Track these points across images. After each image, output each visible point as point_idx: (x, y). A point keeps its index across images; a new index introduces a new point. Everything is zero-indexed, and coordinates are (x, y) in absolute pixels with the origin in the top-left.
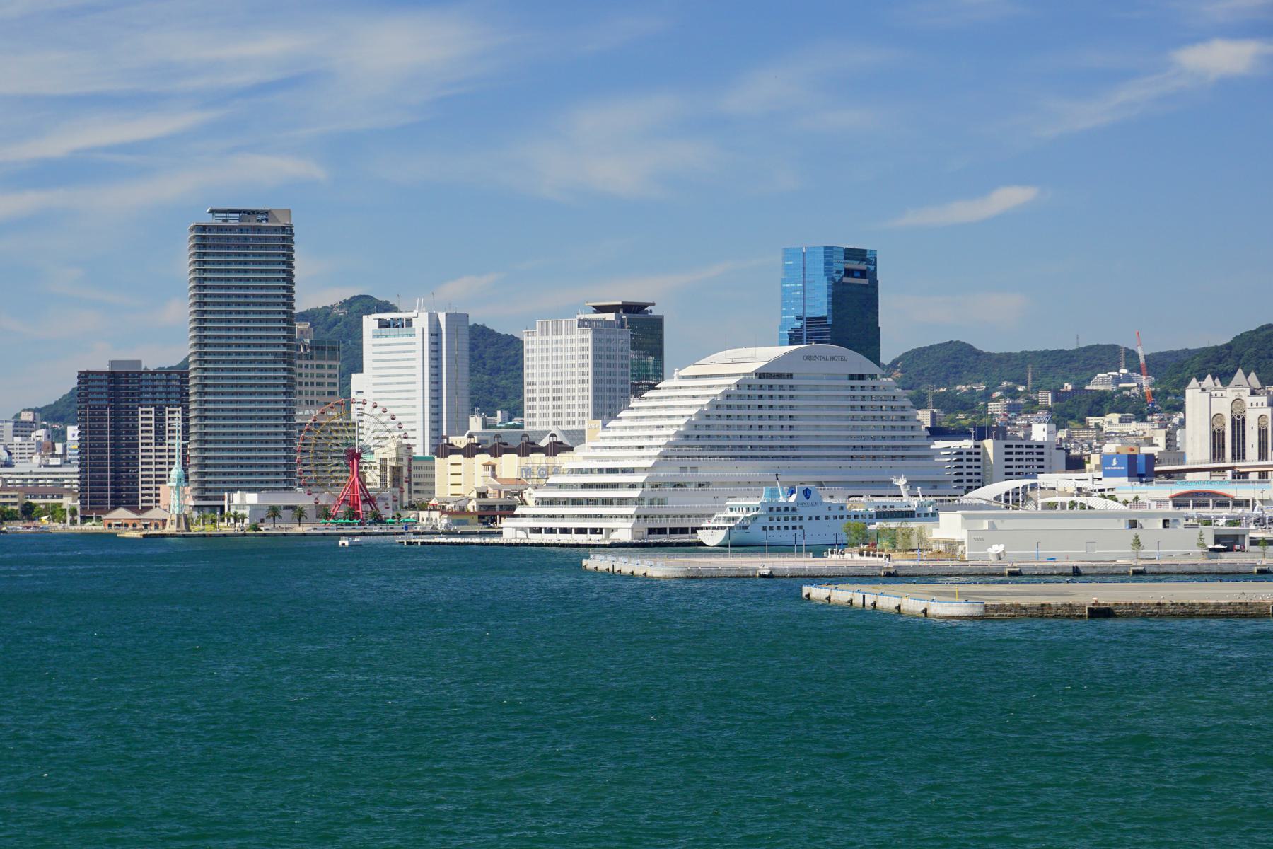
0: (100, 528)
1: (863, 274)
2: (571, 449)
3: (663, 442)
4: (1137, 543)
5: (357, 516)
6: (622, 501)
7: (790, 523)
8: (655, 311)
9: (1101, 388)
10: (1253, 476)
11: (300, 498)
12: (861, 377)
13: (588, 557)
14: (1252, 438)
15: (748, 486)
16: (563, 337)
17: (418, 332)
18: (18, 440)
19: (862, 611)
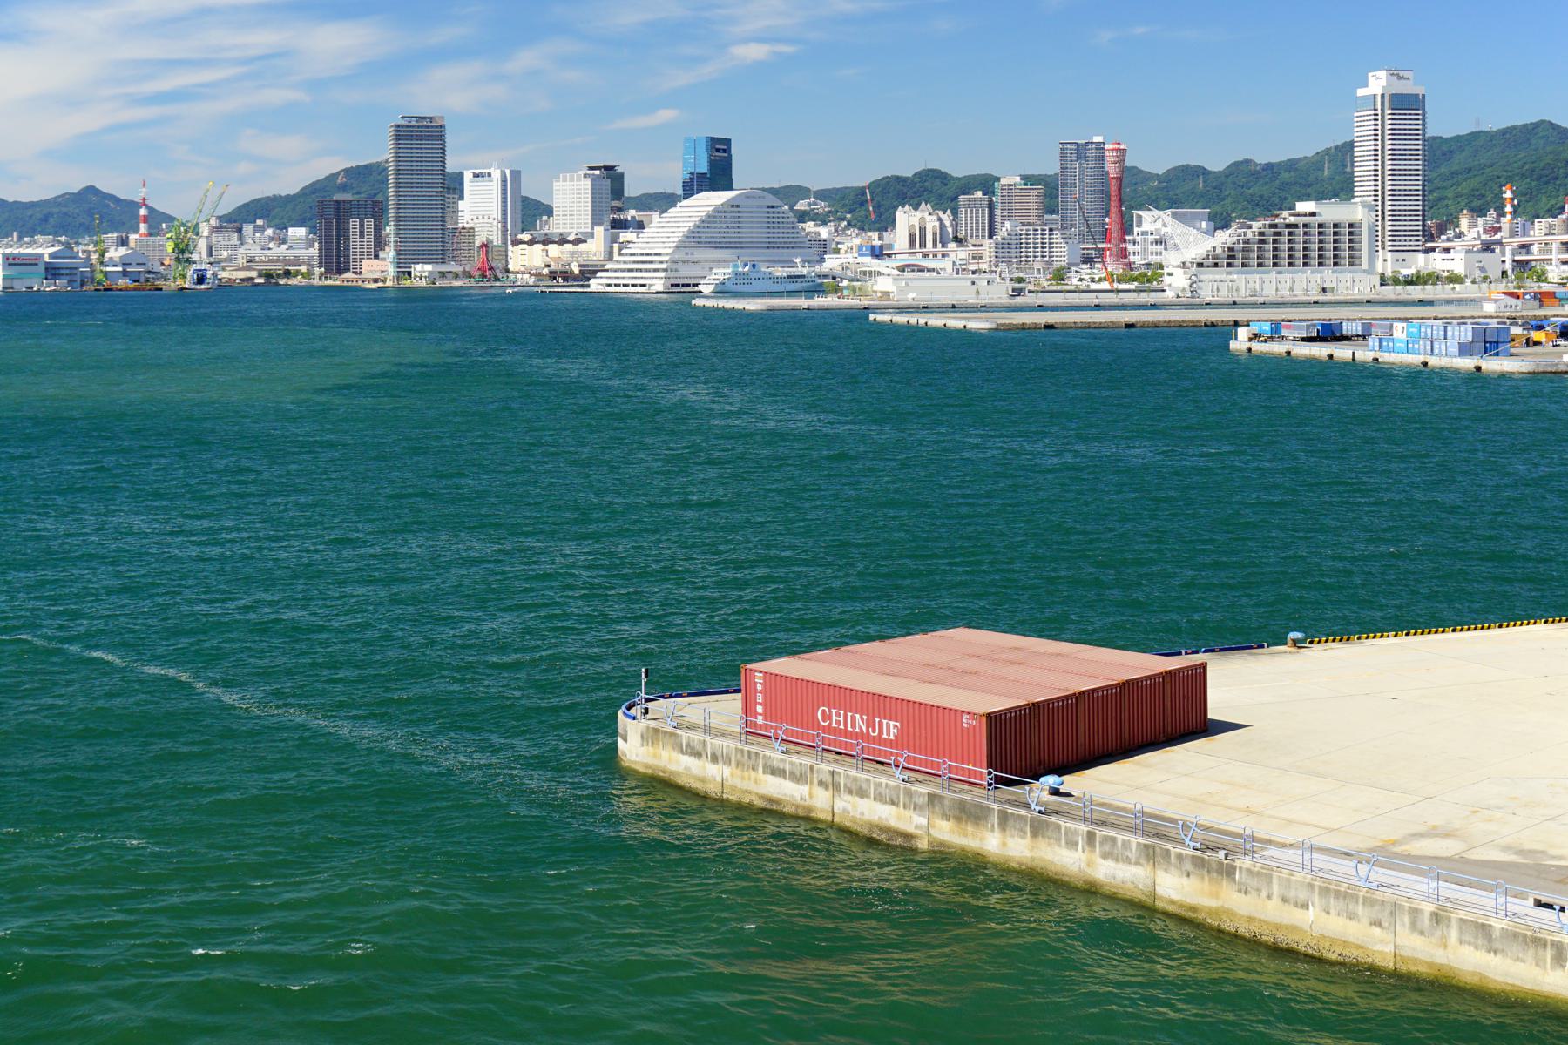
0: (338, 283)
1: (724, 151)
2: (586, 242)
3: (677, 240)
4: (978, 292)
5: (486, 277)
6: (656, 270)
7: (746, 281)
8: (620, 170)
9: (803, 208)
10: (931, 256)
11: (453, 267)
12: (773, 207)
13: (694, 299)
14: (929, 238)
15: (725, 262)
16: (575, 183)
17: (495, 180)
18: (258, 235)
19: (936, 330)
